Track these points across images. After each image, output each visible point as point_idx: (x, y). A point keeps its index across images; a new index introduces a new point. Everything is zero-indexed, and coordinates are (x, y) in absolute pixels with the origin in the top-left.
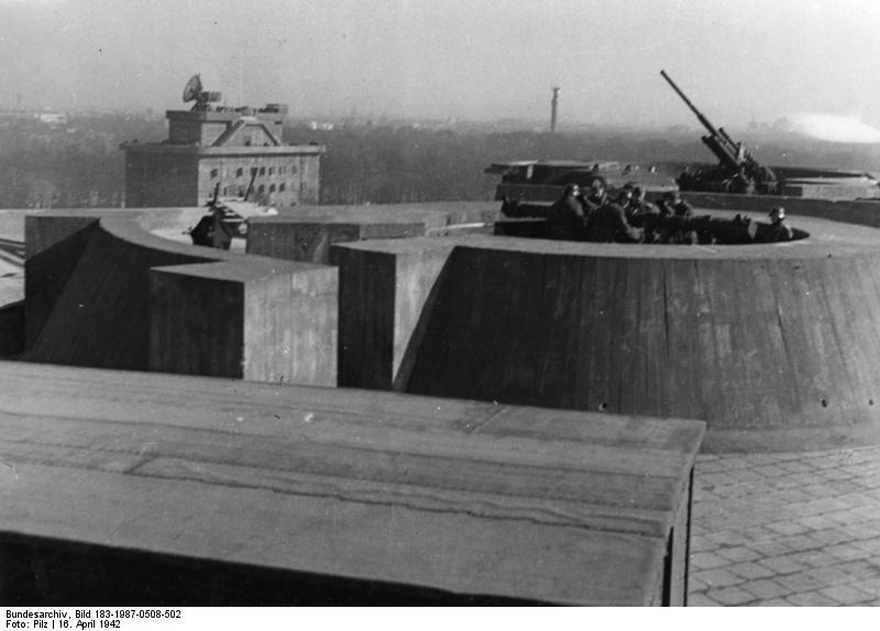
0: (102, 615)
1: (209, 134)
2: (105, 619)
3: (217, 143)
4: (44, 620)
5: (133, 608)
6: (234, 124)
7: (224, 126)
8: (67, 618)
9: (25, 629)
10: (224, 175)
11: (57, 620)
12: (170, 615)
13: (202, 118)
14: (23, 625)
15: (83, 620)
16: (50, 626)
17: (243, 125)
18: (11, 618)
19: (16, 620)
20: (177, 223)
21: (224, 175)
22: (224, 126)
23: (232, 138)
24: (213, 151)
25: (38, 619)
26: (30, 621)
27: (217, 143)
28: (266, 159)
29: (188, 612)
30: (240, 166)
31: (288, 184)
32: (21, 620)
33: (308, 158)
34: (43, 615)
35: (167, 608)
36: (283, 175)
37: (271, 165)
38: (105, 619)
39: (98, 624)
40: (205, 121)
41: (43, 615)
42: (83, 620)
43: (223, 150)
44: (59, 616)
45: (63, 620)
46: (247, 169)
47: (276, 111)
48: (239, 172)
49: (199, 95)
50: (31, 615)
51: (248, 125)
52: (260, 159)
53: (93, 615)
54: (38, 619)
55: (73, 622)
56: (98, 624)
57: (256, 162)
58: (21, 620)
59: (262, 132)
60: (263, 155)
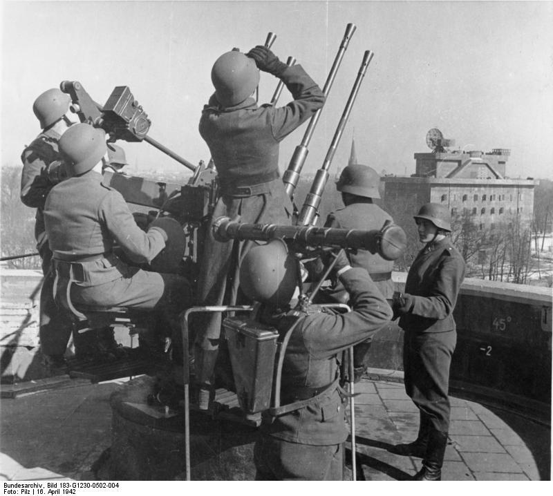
0: (64, 486)
1: (443, 169)
2: (66, 488)
3: (449, 177)
4: (28, 489)
5: (105, 482)
6: (462, 163)
7: (456, 164)
8: (42, 488)
9: (16, 495)
10: (452, 199)
11: (36, 489)
12: (111, 486)
13: (437, 158)
14: (15, 492)
15: (52, 489)
16: (31, 492)
17: (470, 163)
18: (7, 488)
19: (10, 489)
20: (525, 238)
21: (452, 199)
22: (456, 164)
23: (461, 171)
24: (444, 181)
25: (24, 488)
26: (19, 490)
27: (449, 177)
28: (488, 189)
29: (123, 484)
30: (465, 193)
31: (507, 208)
32: (13, 489)
33: (524, 189)
34: (27, 486)
35: (94, 482)
36: (502, 201)
37: (492, 193)
38: (66, 488)
39: (61, 491)
40: (440, 160)
41: (27, 486)
42: (52, 489)
43: (451, 181)
44: (37, 487)
45: (40, 489)
46: (480, 196)
47: (500, 154)
48: (465, 198)
49: (439, 144)
50: (19, 486)
51: (473, 163)
52: (483, 189)
53: (59, 486)
54: (24, 488)
55: (46, 490)
56: (61, 491)
57: (479, 191)
58: (13, 489)
59: (487, 168)
60: (485, 186)
